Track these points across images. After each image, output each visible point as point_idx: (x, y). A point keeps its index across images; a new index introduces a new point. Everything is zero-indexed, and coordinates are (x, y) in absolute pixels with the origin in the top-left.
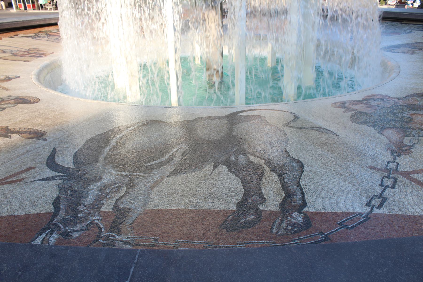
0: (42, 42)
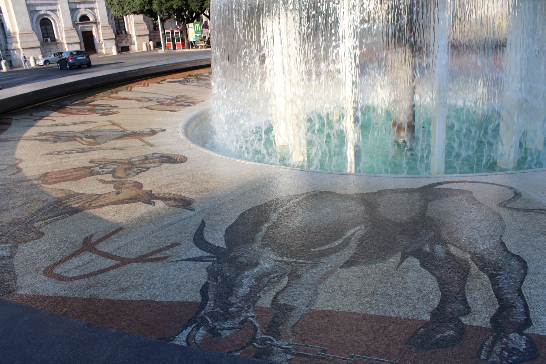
0: (191, 88)
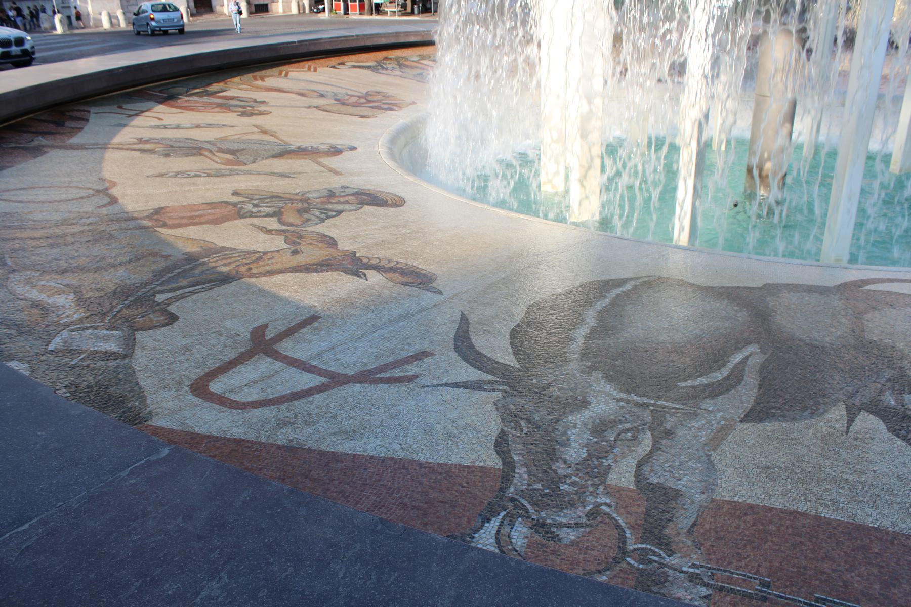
0: (390, 79)
